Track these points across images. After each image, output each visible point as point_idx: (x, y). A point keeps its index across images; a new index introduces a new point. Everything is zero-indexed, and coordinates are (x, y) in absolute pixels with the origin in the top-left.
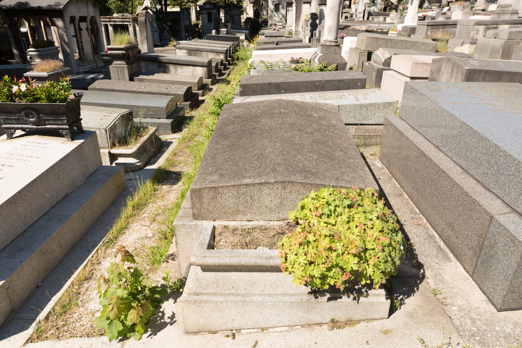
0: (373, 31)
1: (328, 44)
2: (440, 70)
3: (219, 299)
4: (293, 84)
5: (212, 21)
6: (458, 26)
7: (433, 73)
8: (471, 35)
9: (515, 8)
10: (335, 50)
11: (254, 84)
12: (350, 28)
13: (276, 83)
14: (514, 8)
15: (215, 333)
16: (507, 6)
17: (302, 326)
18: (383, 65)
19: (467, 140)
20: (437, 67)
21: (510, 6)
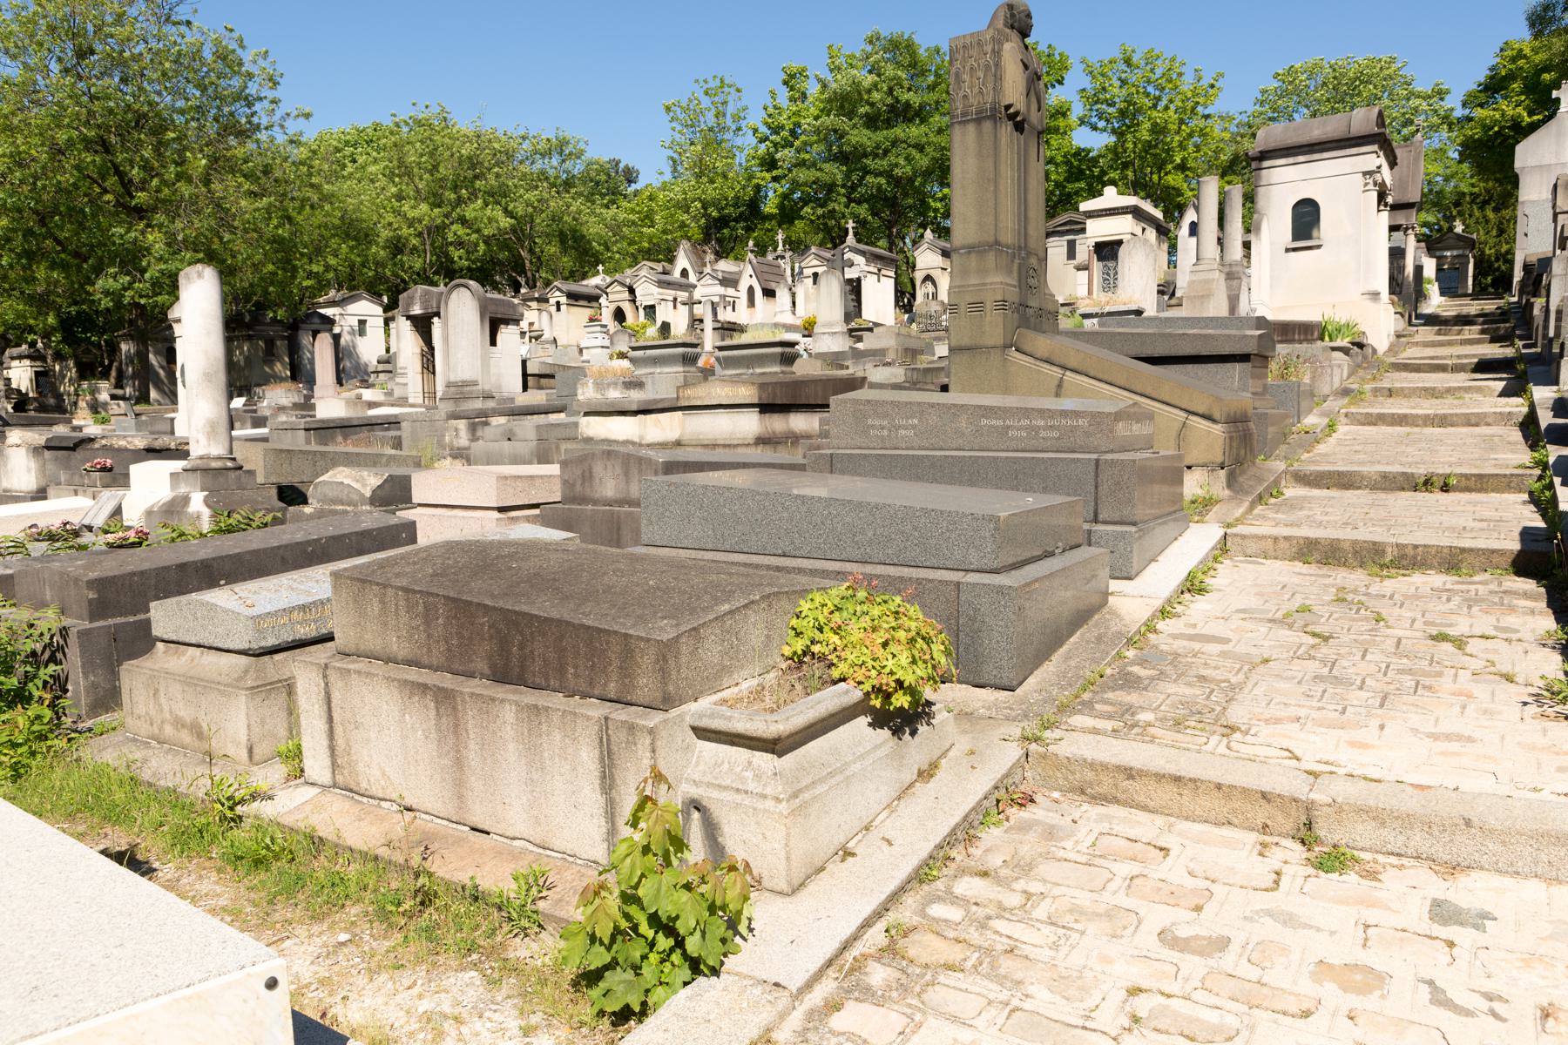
0: (168, 449)
1: (214, 464)
2: (591, 476)
3: (820, 789)
4: (248, 557)
5: (1527, 267)
6: (403, 424)
7: (573, 485)
8: (447, 439)
9: (487, 387)
10: (239, 478)
11: (134, 574)
12: (97, 446)
13: (202, 561)
14: (485, 385)
15: (822, 869)
16: (465, 384)
17: (899, 798)
18: (372, 504)
19: (848, 519)
20: (579, 472)
21: (475, 383)
